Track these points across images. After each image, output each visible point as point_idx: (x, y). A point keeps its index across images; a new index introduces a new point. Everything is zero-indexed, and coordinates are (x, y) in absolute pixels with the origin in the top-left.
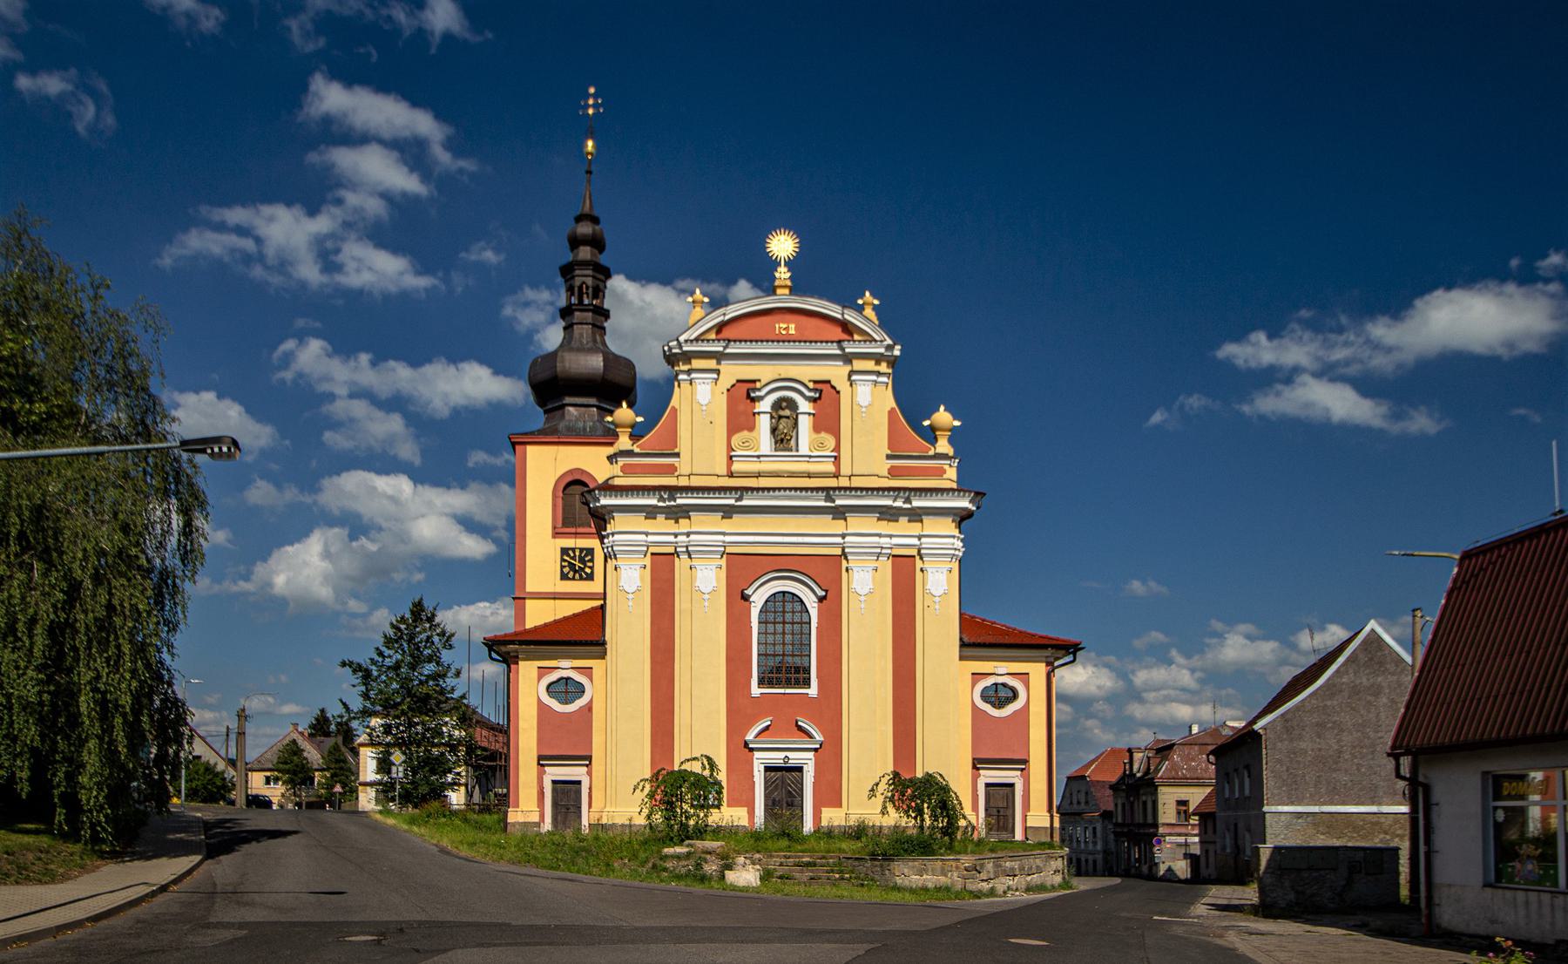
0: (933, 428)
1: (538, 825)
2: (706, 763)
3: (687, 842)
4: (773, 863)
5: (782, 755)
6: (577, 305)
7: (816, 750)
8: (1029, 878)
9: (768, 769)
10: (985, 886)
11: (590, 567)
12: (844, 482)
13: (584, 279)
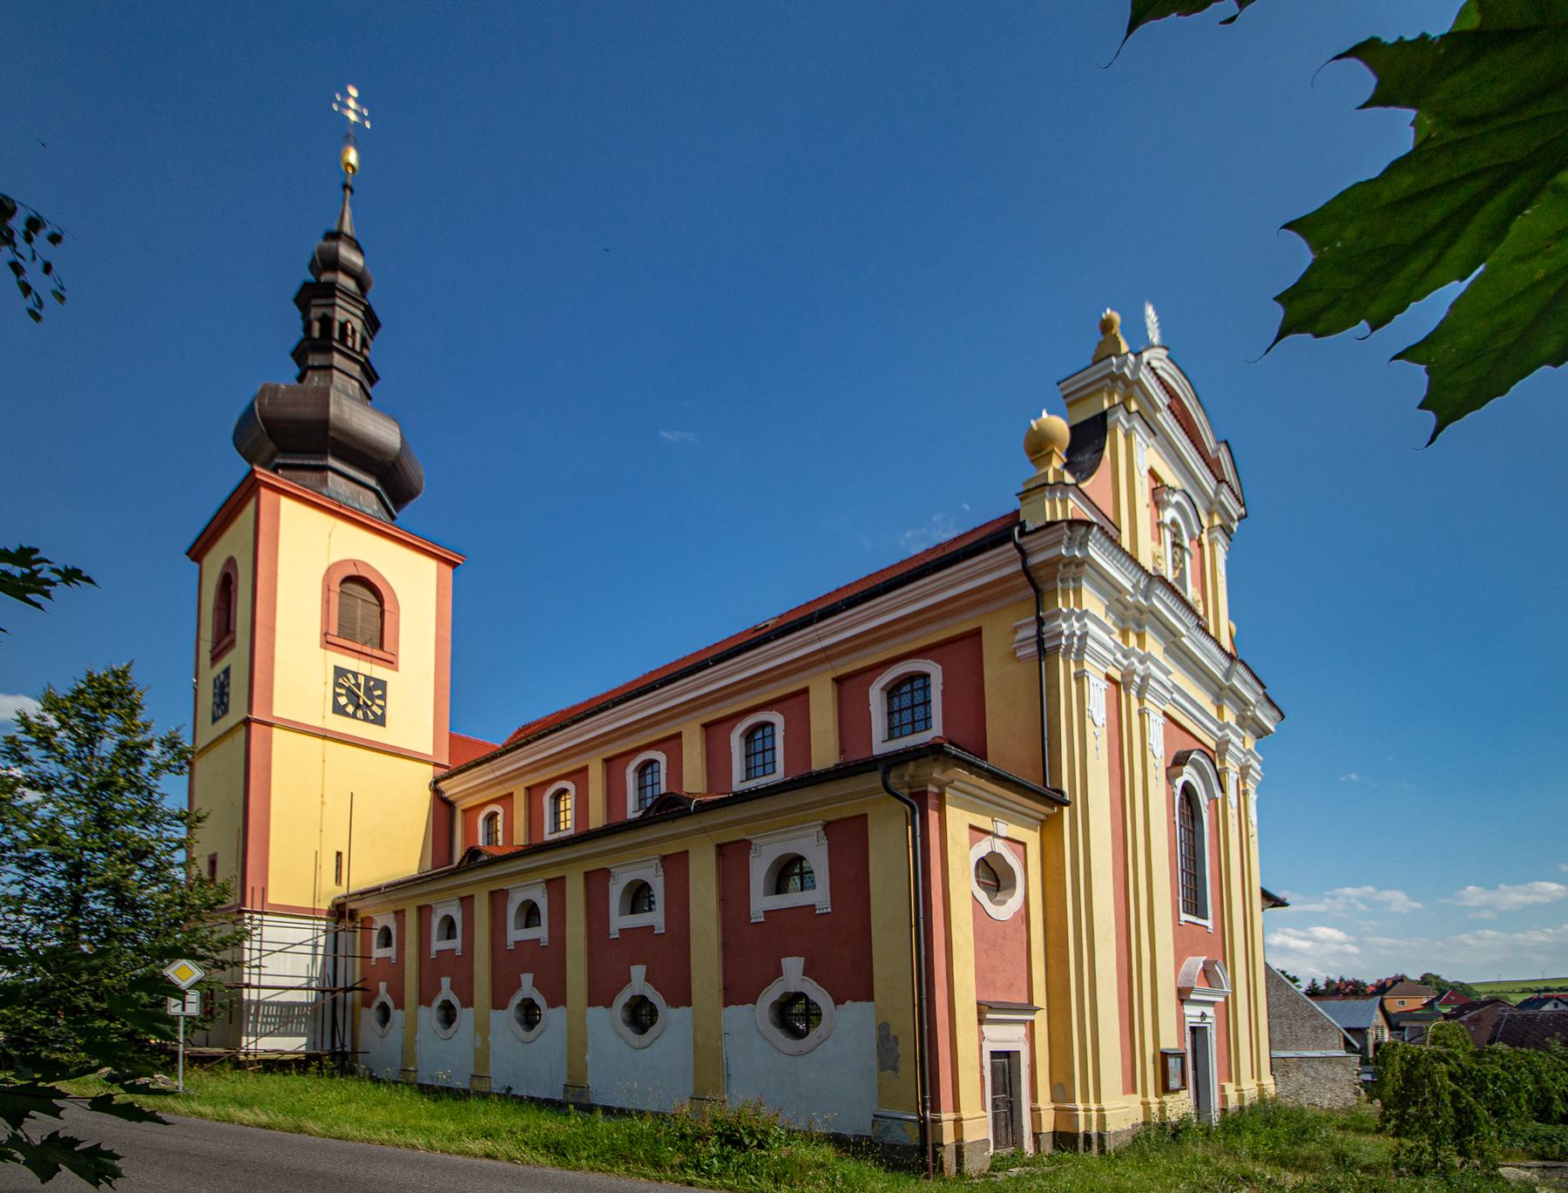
6: (337, 341)
11: (379, 706)
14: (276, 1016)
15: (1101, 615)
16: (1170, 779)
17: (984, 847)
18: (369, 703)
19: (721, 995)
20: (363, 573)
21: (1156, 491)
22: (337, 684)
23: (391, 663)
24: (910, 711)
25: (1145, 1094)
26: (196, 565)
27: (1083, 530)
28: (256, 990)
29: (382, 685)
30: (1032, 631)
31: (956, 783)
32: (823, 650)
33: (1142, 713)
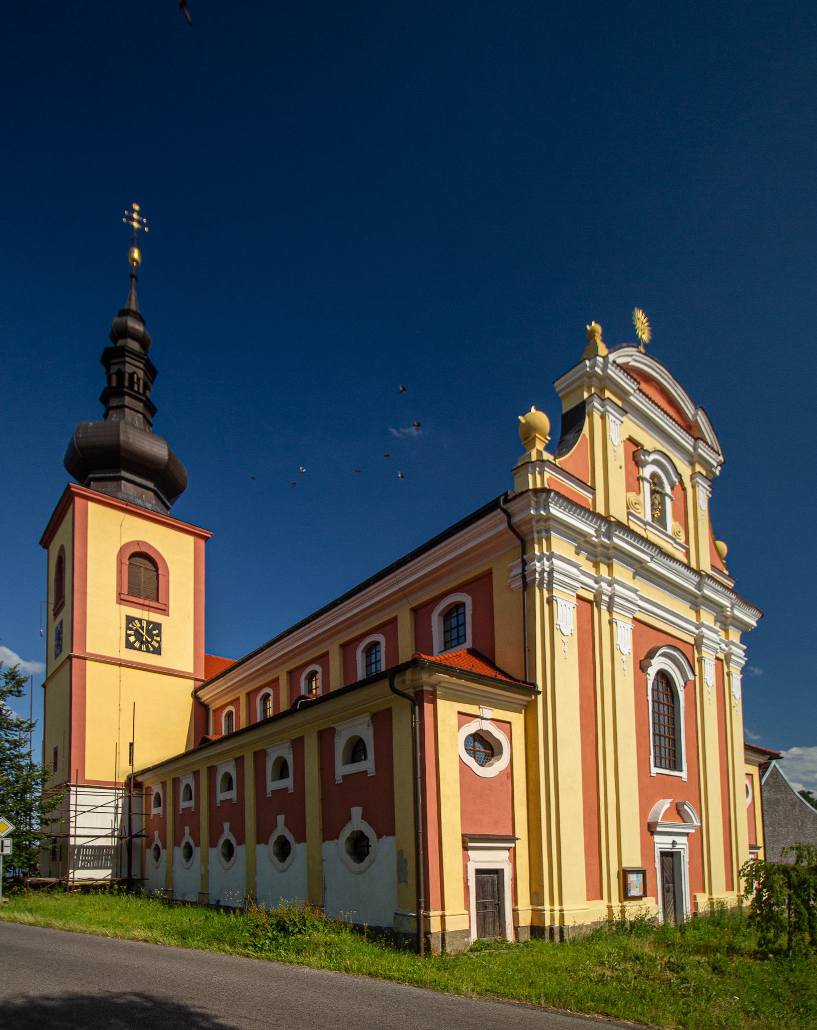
6: (127, 388)
11: (157, 641)
13: (136, 369)
14: (91, 856)
15: (573, 557)
16: (642, 666)
17: (473, 727)
18: (149, 640)
20: (144, 549)
21: (636, 454)
22: (128, 628)
23: (165, 611)
24: (456, 630)
25: (610, 900)
26: (46, 550)
27: (544, 495)
28: (74, 838)
29: (158, 626)
30: (520, 570)
31: (442, 684)
32: (401, 589)
33: (611, 623)
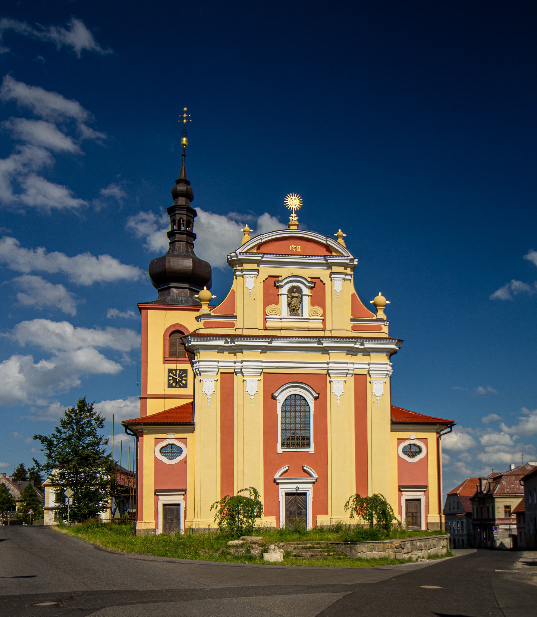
0: (375, 305)
1: (154, 530)
2: (252, 491)
3: (242, 537)
4: (291, 548)
5: (295, 486)
7: (314, 483)
8: (429, 551)
9: (287, 494)
10: (406, 556)
11: (185, 380)
12: (328, 334)
13: (181, 216)
19: (111, 361)
20: (181, 329)
